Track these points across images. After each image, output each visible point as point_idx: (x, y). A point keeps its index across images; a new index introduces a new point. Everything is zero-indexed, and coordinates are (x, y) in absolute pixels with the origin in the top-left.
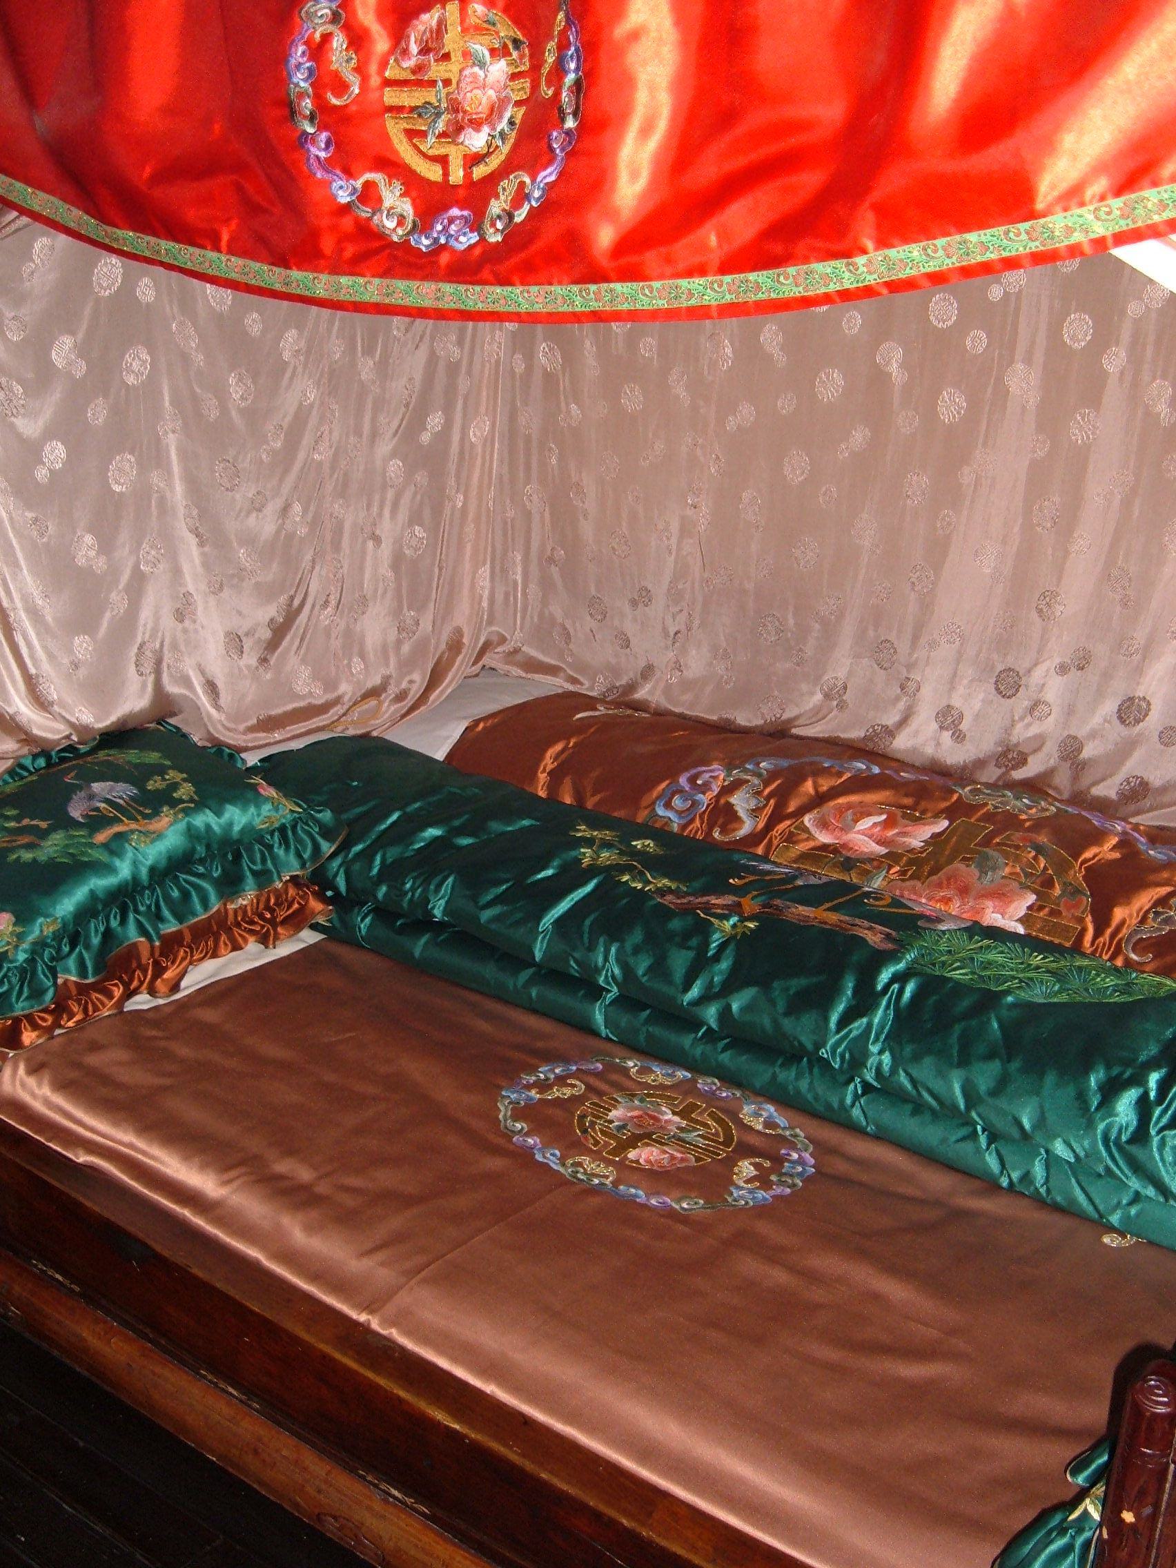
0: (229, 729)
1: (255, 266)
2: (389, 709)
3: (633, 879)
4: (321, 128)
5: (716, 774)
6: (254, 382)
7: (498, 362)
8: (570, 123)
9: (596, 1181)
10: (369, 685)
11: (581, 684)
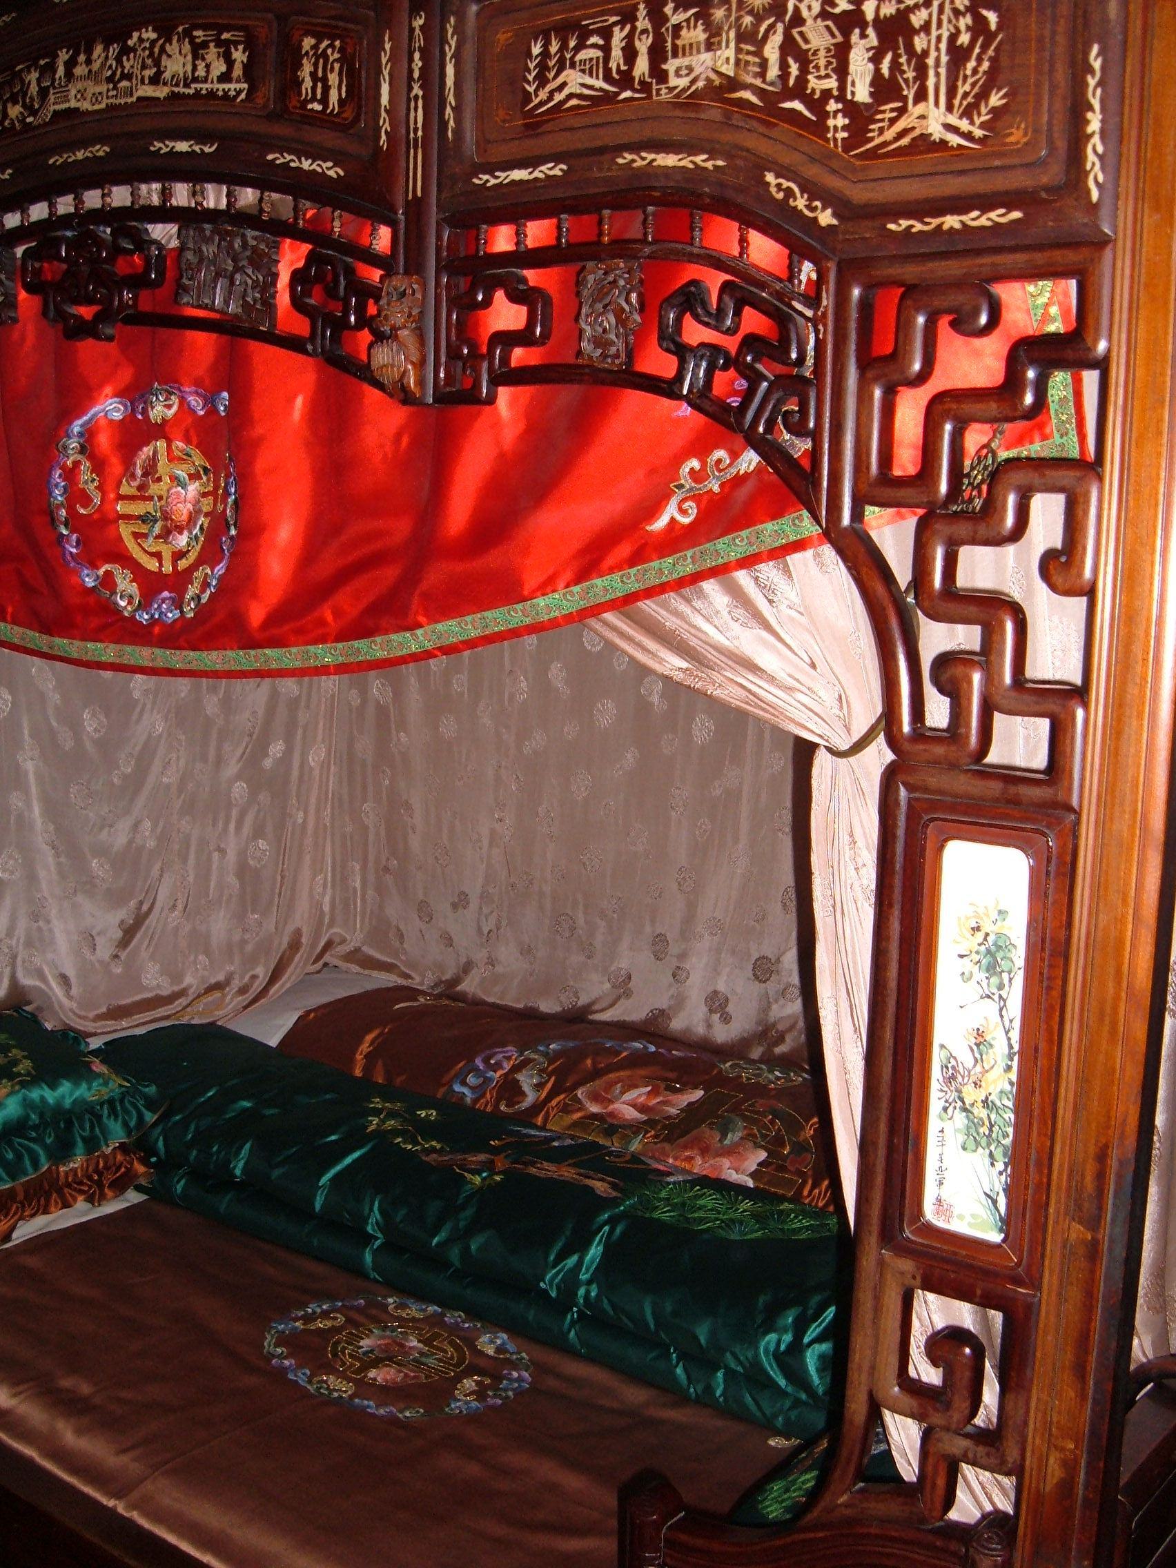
0: (80, 1017)
1: (30, 633)
2: (233, 1001)
3: (405, 1142)
4: (72, 532)
5: (506, 1057)
6: (107, 716)
7: (333, 696)
8: (233, 532)
9: (336, 1394)
10: (213, 981)
11: (412, 978)
